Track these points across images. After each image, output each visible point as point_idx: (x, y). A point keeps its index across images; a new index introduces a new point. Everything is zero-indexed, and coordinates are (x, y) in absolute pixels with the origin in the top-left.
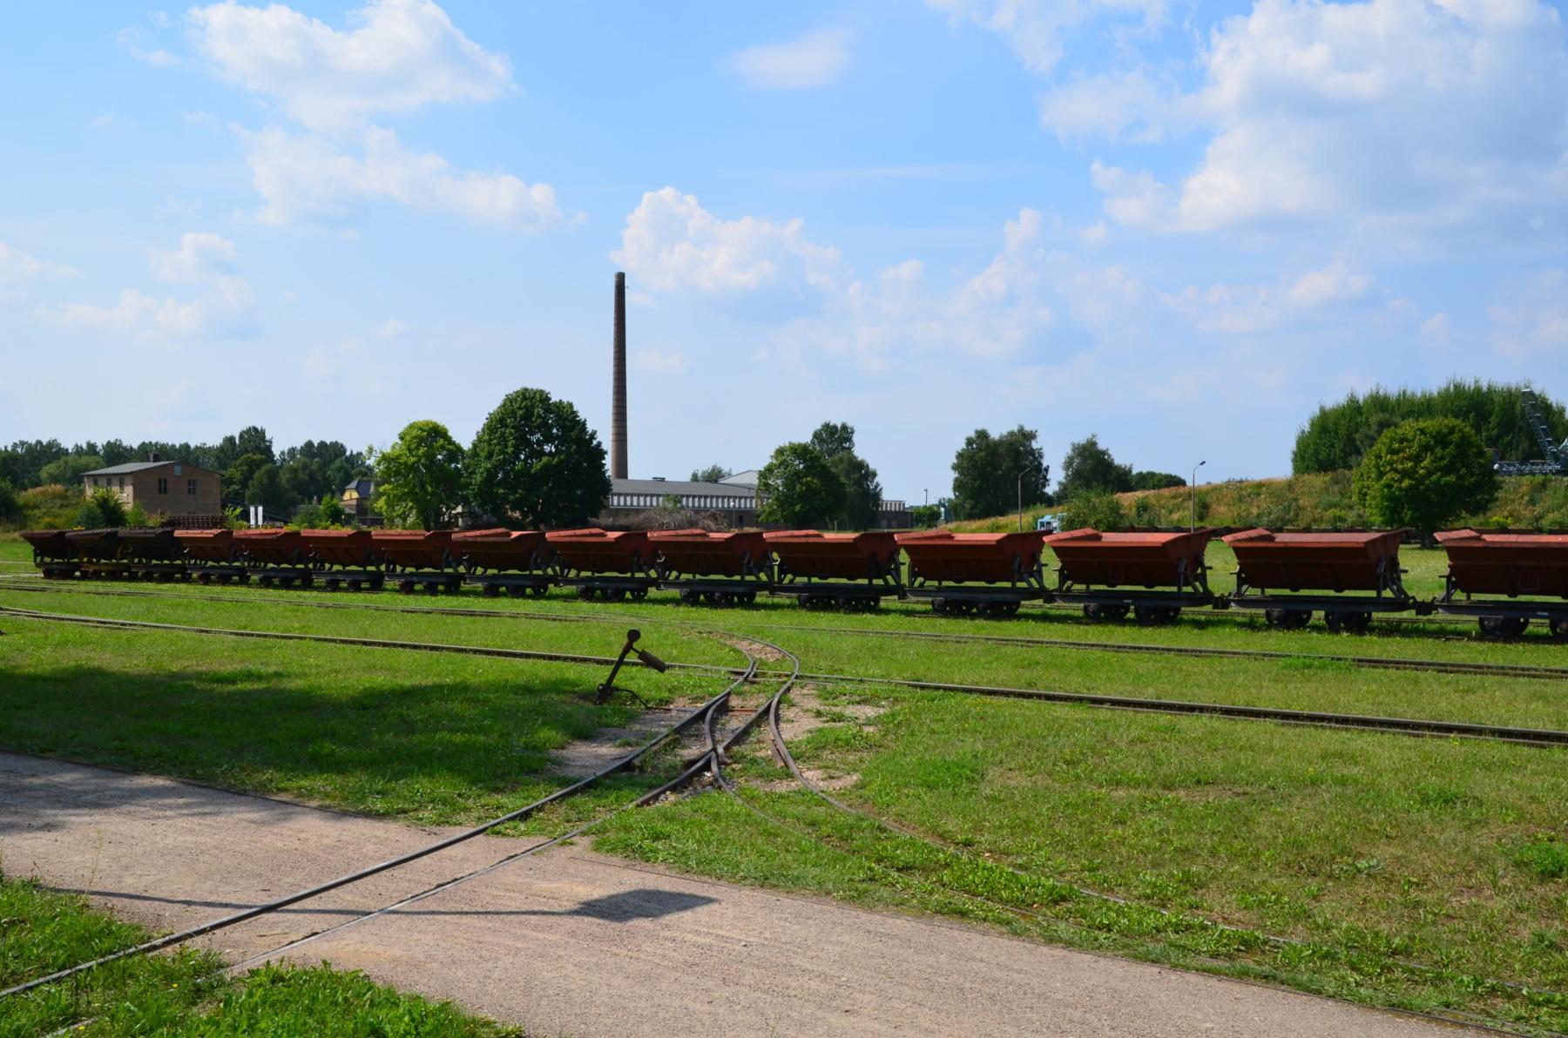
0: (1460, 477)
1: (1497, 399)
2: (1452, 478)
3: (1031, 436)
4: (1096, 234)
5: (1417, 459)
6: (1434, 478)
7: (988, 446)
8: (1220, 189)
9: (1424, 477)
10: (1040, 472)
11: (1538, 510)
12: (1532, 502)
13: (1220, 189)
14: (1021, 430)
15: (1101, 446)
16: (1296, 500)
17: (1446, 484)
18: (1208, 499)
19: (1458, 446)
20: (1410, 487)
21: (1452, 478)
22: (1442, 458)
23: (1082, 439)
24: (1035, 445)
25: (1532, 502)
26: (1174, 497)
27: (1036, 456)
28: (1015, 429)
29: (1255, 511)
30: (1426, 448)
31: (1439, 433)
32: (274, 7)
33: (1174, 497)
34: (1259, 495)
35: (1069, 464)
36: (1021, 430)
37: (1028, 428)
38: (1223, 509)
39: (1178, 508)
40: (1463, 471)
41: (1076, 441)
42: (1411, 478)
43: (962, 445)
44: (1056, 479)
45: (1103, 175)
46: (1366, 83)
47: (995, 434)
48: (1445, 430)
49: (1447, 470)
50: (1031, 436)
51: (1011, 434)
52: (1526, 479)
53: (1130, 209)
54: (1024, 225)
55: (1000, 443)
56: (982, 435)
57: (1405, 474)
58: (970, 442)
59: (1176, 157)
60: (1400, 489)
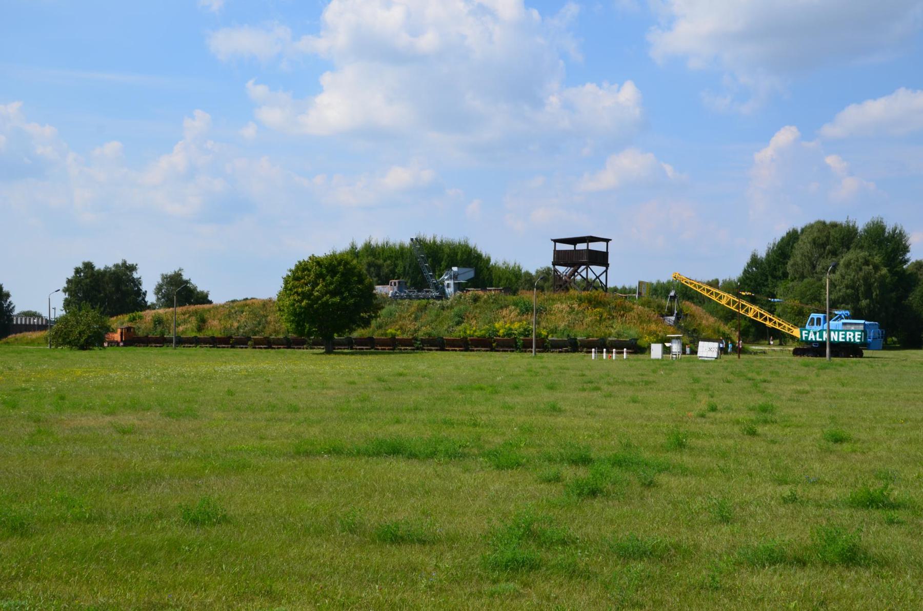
0: (343, 299)
1: (447, 250)
2: (337, 299)
3: (133, 268)
4: (250, 132)
5: (315, 284)
6: (325, 299)
7: (93, 275)
8: (335, 107)
9: (318, 298)
10: (140, 294)
11: (418, 324)
12: (416, 319)
13: (335, 107)
14: (124, 263)
15: (185, 277)
16: (266, 316)
17: (333, 304)
18: (206, 316)
19: (343, 275)
20: (309, 306)
21: (337, 299)
22: (331, 283)
23: (170, 272)
24: (135, 275)
25: (416, 319)
26: (184, 314)
27: (137, 283)
28: (120, 262)
29: (236, 324)
30: (320, 276)
31: (330, 264)
32: (787, 127)
33: (184, 314)
34: (242, 312)
35: (159, 289)
36: (124, 263)
37: (129, 262)
38: (216, 322)
39: (185, 322)
40: (346, 294)
41: (165, 273)
42: (309, 299)
43: (71, 274)
44: (151, 298)
45: (257, 91)
46: (428, 41)
47: (99, 266)
48: (335, 263)
49: (333, 294)
50: (133, 268)
51: (116, 266)
52: (416, 303)
53: (272, 116)
54: (198, 122)
55: (99, 272)
56: (88, 266)
57: (304, 296)
58: (77, 271)
59: (303, 80)
60: (301, 307)
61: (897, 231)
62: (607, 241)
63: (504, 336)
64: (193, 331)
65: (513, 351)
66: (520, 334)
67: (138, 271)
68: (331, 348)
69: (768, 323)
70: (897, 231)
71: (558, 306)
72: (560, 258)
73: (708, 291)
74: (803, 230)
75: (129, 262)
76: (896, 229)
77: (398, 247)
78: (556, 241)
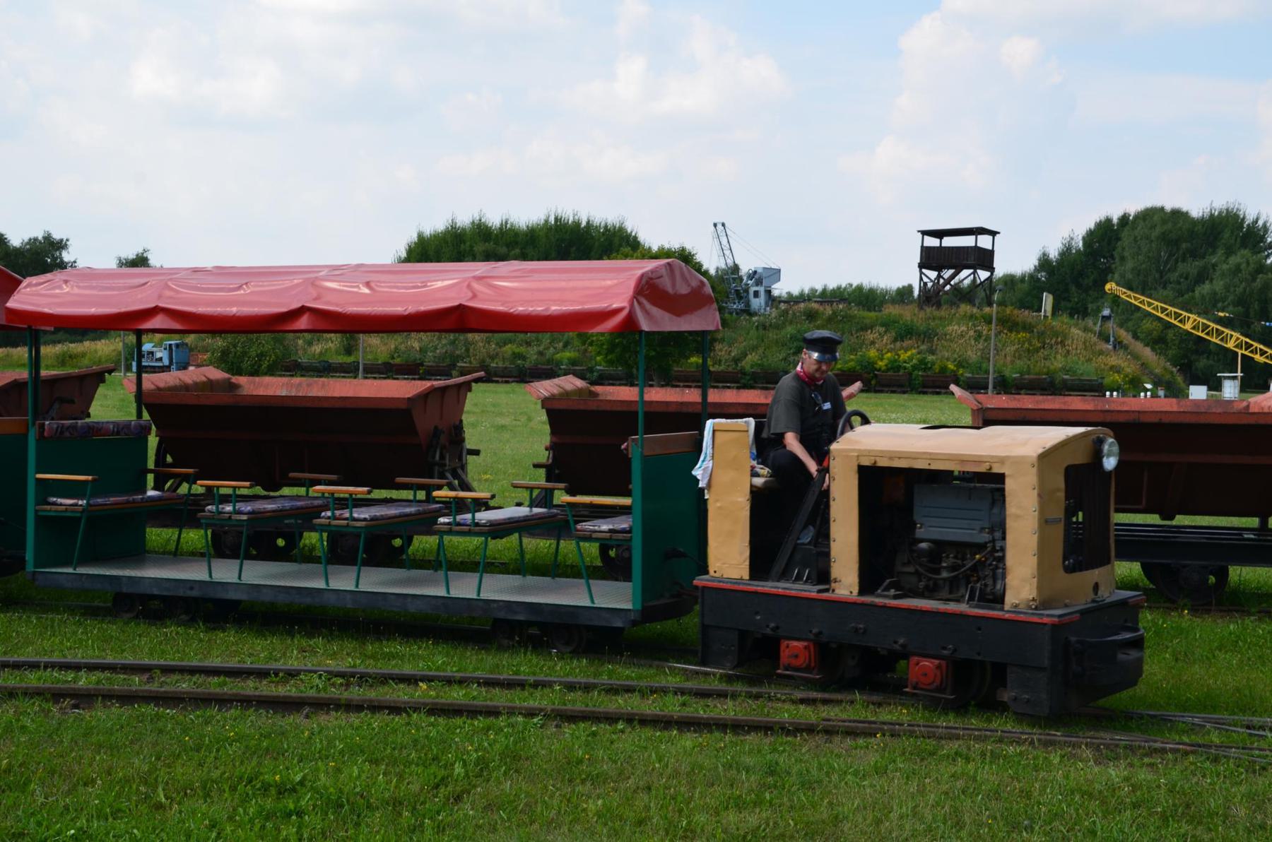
3: (61, 245)
50: (61, 245)
61: (1260, 223)
62: (993, 234)
63: (888, 370)
64: (338, 353)
65: (904, 392)
66: (915, 367)
67: (70, 249)
68: (272, 375)
69: (1257, 357)
70: (1260, 223)
71: (954, 328)
72: (930, 259)
73: (1163, 310)
74: (1137, 216)
75: (57, 236)
76: (1257, 219)
77: (584, 224)
78: (924, 233)
